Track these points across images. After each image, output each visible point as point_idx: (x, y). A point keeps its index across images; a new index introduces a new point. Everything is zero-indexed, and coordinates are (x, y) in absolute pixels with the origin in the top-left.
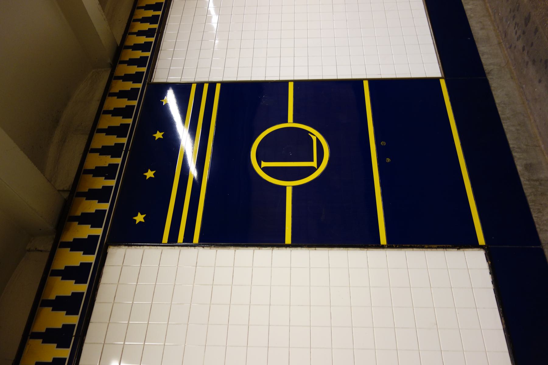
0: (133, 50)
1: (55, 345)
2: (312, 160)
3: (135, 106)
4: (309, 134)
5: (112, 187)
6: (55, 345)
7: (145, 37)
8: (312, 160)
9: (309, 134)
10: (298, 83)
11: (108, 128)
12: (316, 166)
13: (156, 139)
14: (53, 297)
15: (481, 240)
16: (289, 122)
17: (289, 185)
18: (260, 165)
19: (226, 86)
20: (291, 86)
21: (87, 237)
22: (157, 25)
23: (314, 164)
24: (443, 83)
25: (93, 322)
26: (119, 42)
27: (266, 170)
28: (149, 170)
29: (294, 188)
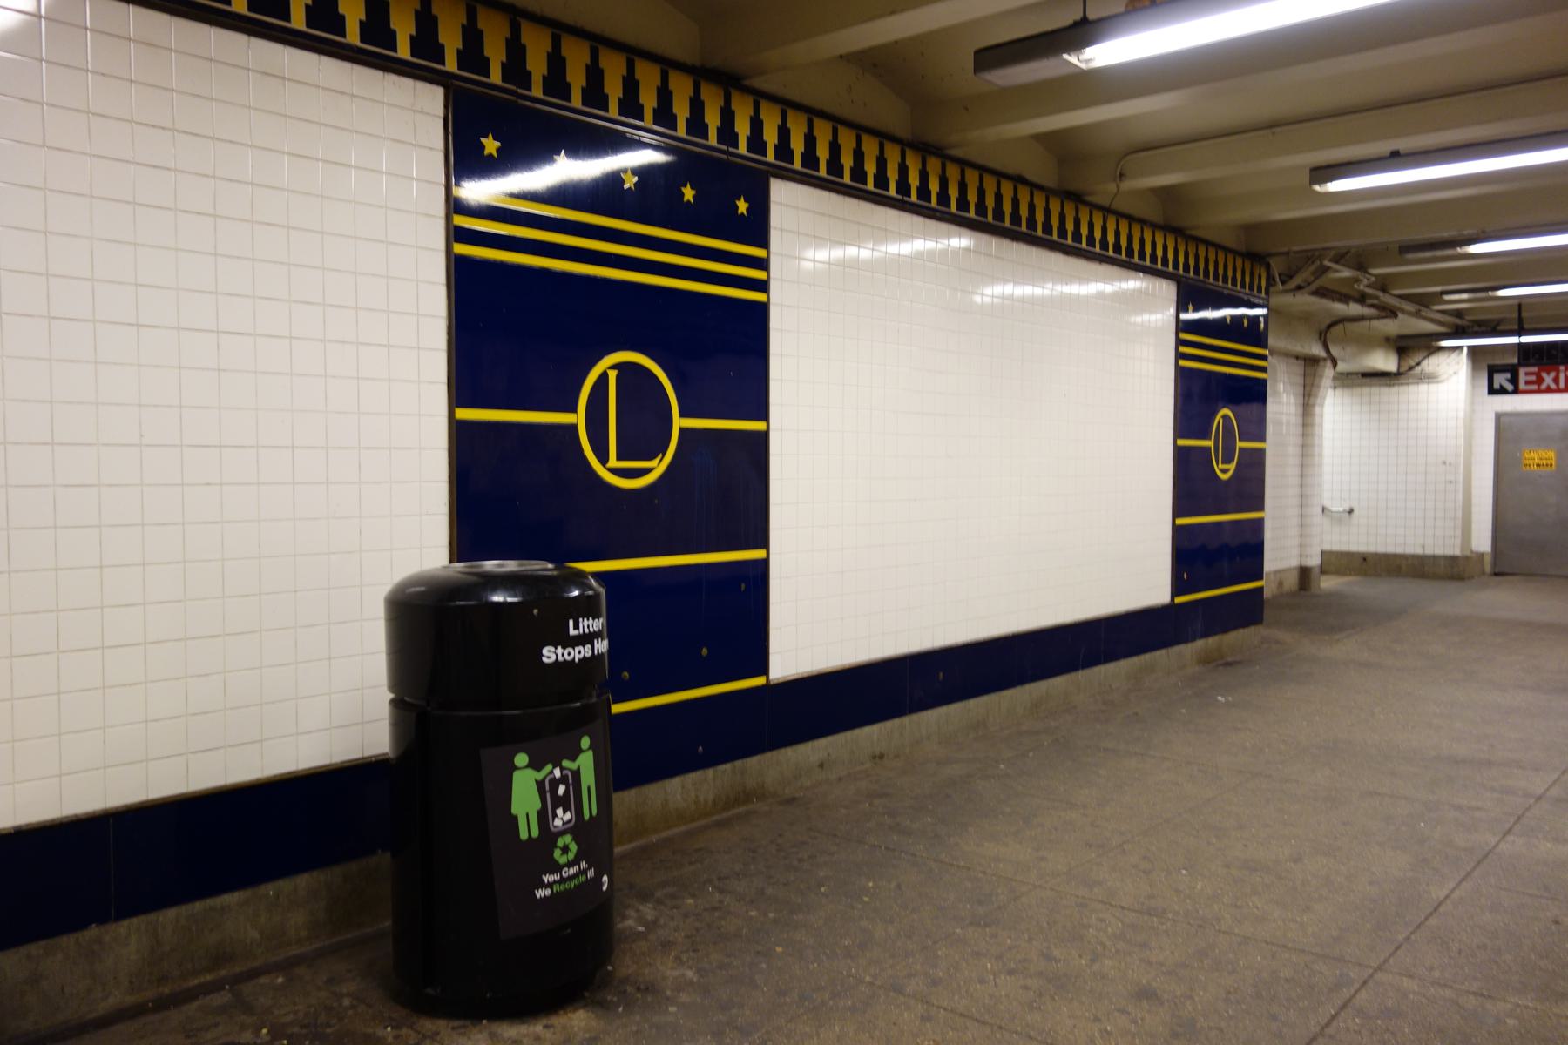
2: (619, 458)
8: (619, 458)
9: (661, 455)
10: (763, 438)
13: (483, 140)
15: (1178, 600)
17: (579, 418)
18: (612, 367)
19: (762, 310)
20: (758, 426)
23: (613, 462)
24: (759, 681)
25: (249, 42)
26: (747, 82)
27: (604, 377)
28: (498, 144)
29: (574, 427)
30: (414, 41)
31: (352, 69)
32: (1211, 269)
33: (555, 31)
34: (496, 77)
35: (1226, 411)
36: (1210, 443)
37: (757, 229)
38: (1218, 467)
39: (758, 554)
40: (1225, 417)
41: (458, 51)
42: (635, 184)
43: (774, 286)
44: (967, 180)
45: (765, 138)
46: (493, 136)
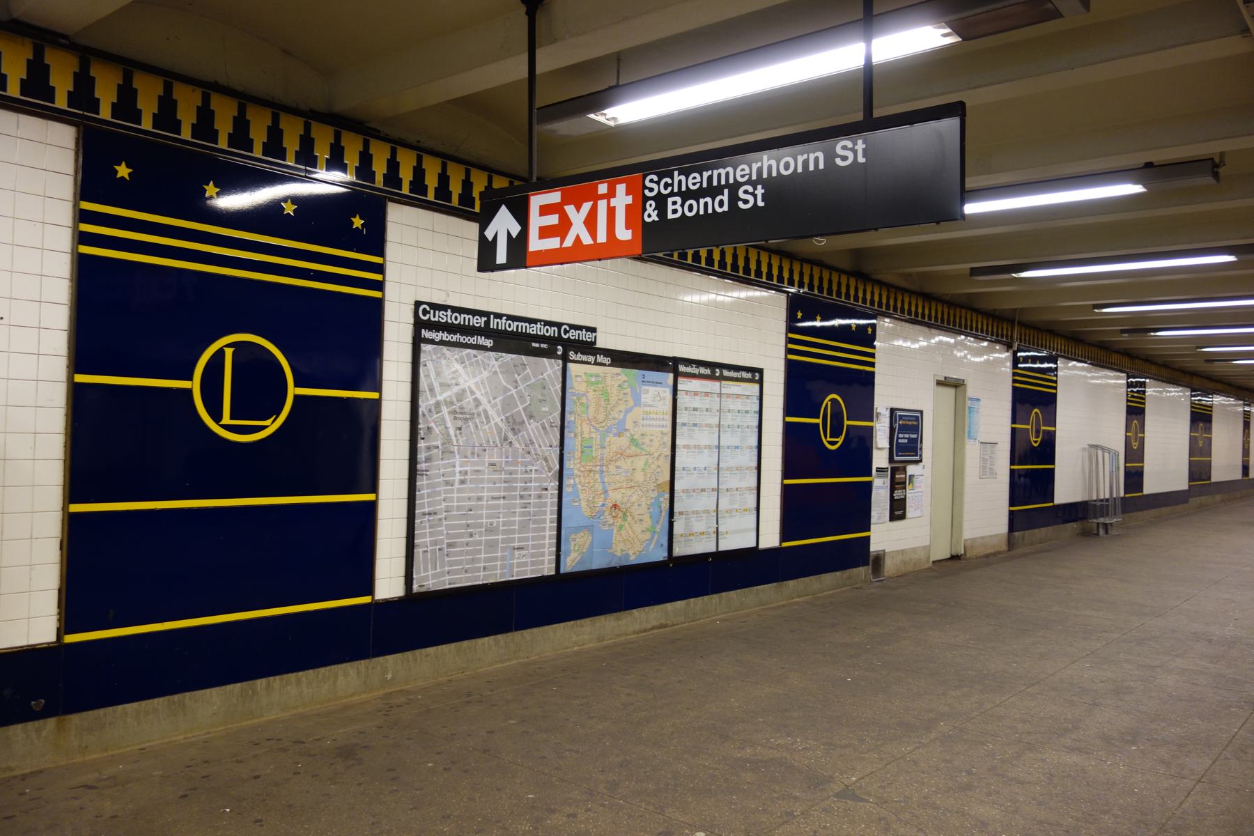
0: (463, 183)
1: (71, 89)
3: (180, 135)
4: (275, 416)
5: (54, 103)
6: (115, 101)
7: (437, 186)
9: (275, 416)
11: (211, 110)
12: (222, 422)
14: (47, 60)
15: (70, 639)
16: (296, 388)
17: (195, 385)
18: (228, 346)
20: (789, 419)
21: (51, 84)
22: (190, 136)
23: (226, 420)
24: (366, 600)
25: (47, 126)
26: (875, 277)
27: (220, 354)
30: (114, 107)
31: (47, 123)
32: (946, 317)
33: (204, 90)
34: (186, 134)
35: (1036, 410)
36: (1029, 427)
37: (375, 240)
38: (1033, 439)
39: (787, 482)
40: (1036, 413)
41: (69, 92)
42: (205, 191)
43: (1147, 404)
44: (833, 278)
45: (739, 264)
46: (359, 216)
